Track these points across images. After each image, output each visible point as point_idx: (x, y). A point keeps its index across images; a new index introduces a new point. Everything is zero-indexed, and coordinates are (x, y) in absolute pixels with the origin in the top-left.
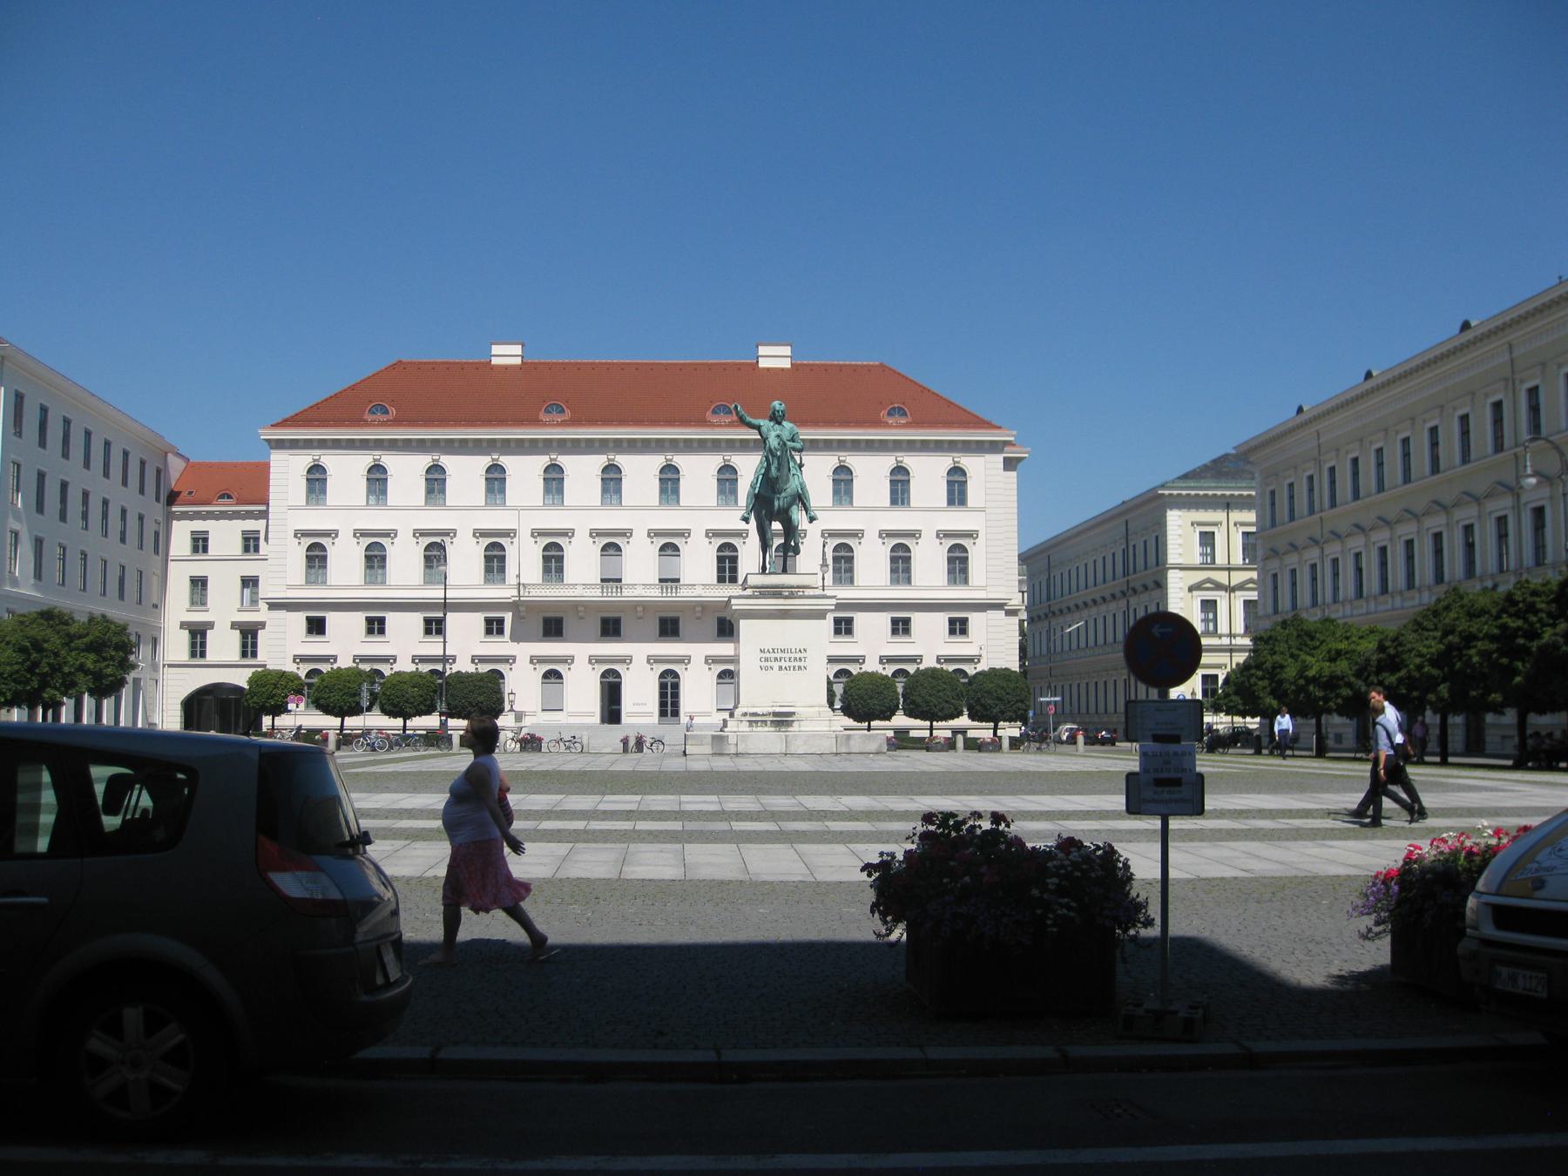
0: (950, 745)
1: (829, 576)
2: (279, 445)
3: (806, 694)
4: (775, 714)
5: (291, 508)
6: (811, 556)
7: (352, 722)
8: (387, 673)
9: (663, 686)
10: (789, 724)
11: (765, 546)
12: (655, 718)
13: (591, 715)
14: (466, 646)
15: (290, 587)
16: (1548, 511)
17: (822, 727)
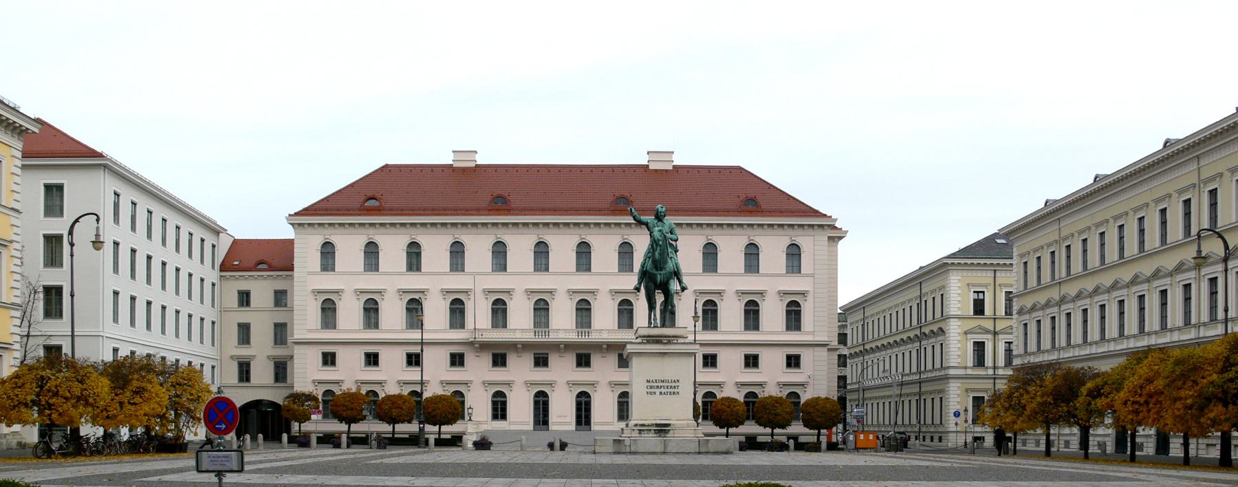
0: (782, 447)
1: (700, 324)
3: (678, 410)
4: (657, 425)
5: (310, 273)
6: (686, 309)
7: (354, 427)
8: (338, 392)
9: (579, 404)
10: (666, 432)
11: (652, 307)
12: (573, 427)
13: (527, 424)
14: (436, 377)
15: (310, 331)
16: (1193, 287)
17: (690, 434)
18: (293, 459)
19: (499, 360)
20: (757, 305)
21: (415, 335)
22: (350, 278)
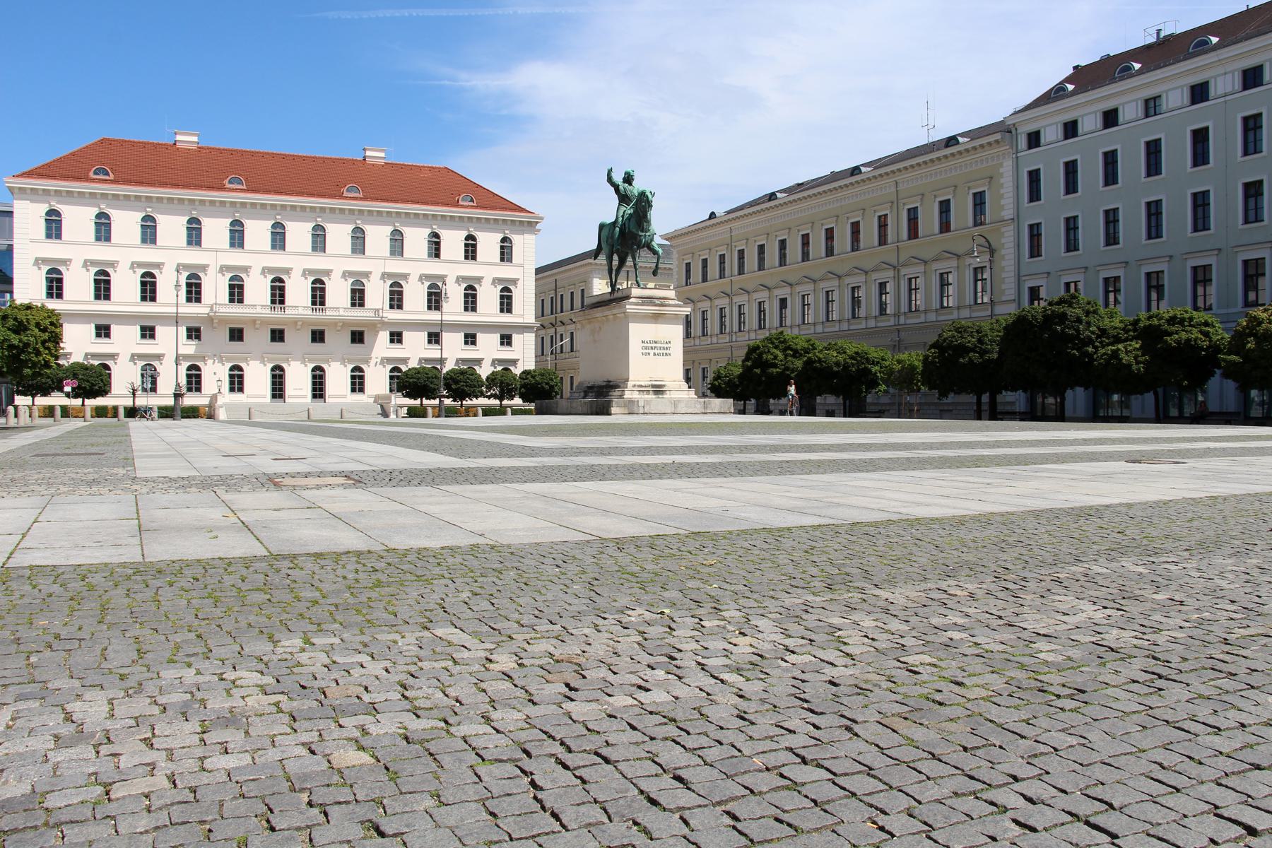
2: (23, 193)
4: (653, 386)
5: (32, 241)
21: (434, 316)
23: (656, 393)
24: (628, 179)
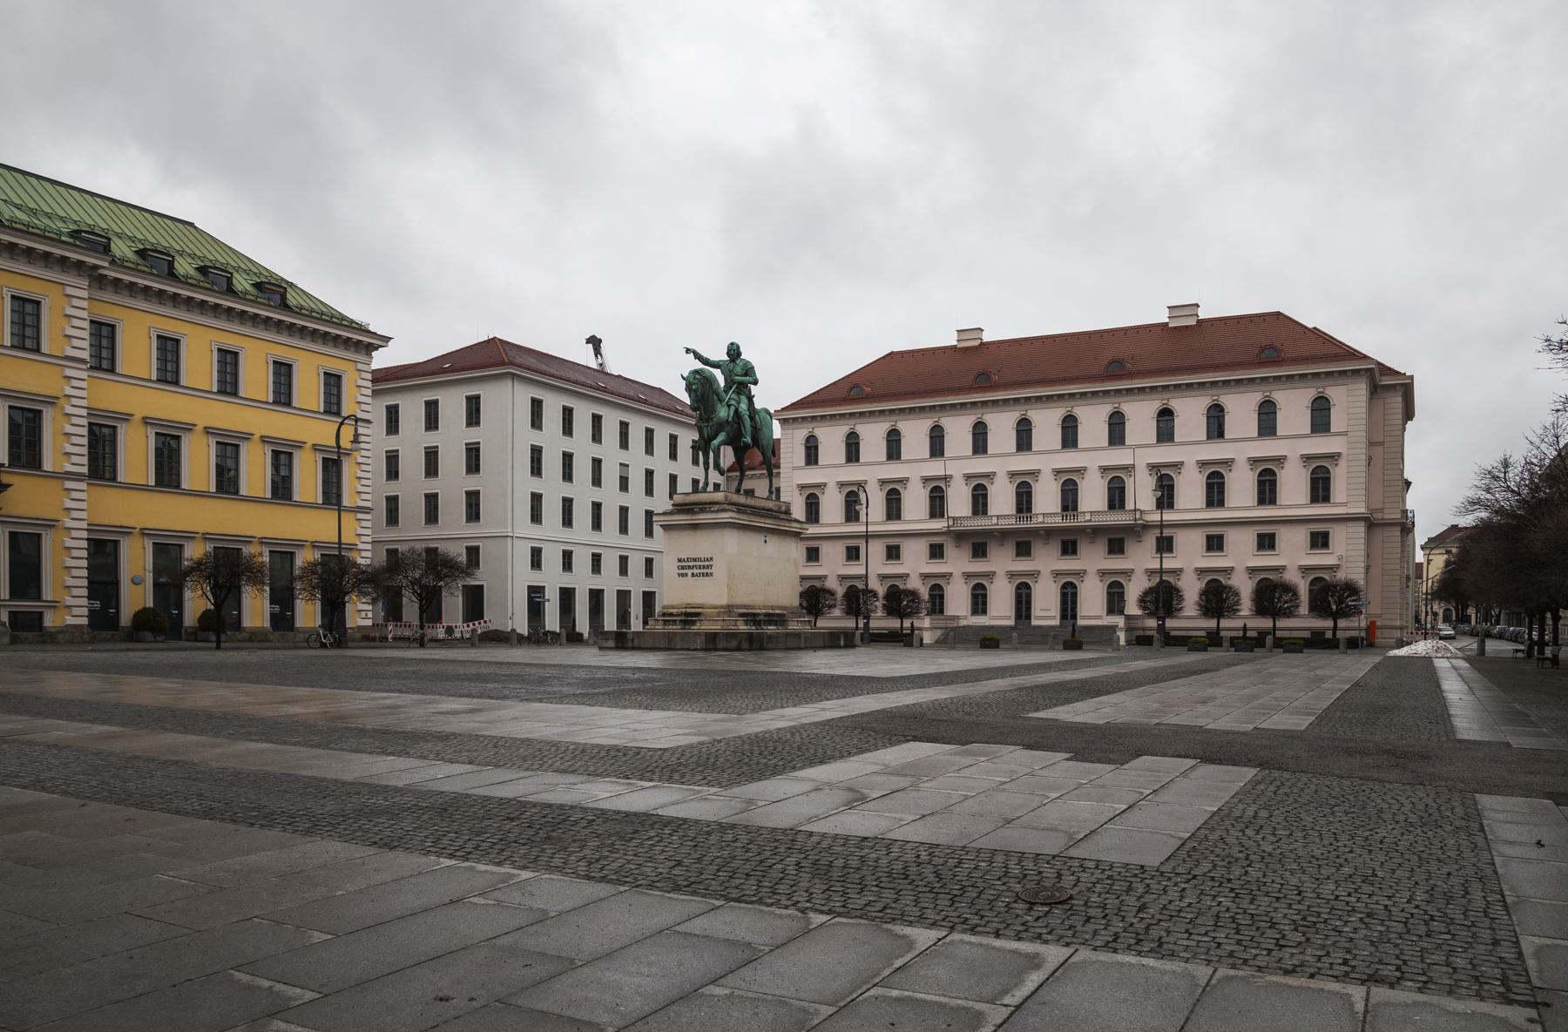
5: (795, 468)
9: (1064, 595)
13: (1008, 618)
14: (915, 565)
18: (375, 699)
19: (979, 551)
20: (1328, 471)
22: (832, 472)
23: (685, 622)
24: (734, 352)
